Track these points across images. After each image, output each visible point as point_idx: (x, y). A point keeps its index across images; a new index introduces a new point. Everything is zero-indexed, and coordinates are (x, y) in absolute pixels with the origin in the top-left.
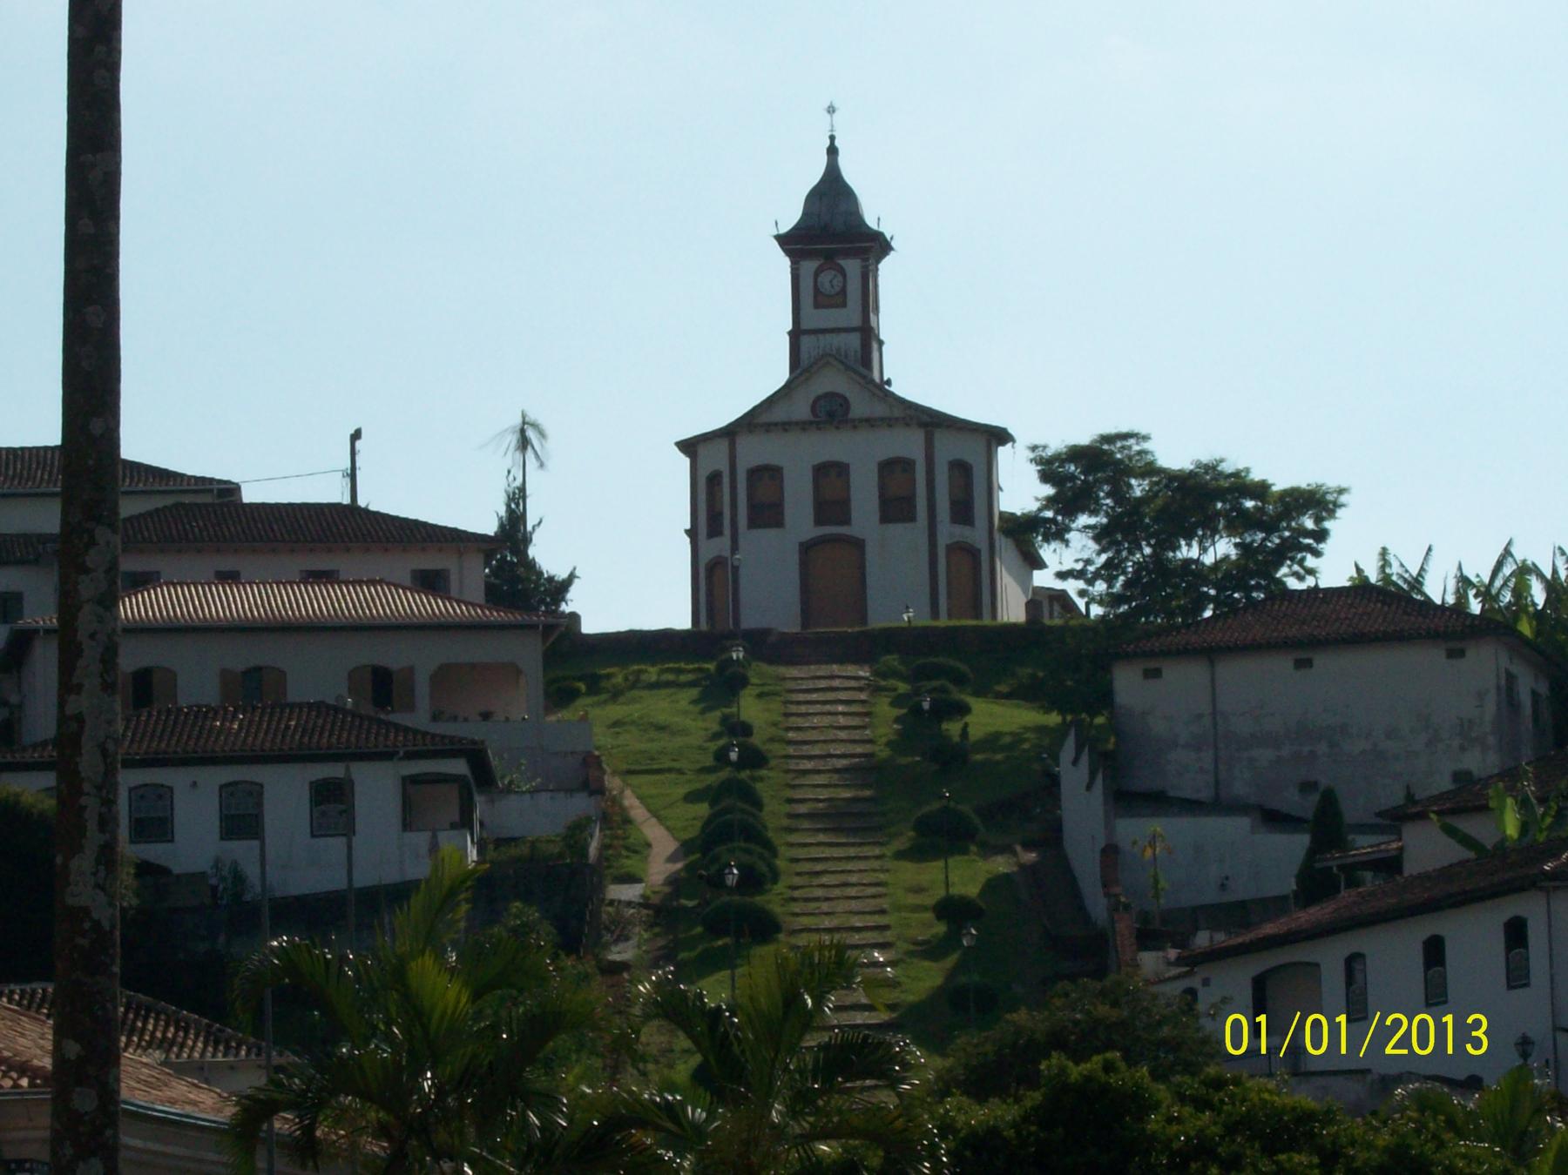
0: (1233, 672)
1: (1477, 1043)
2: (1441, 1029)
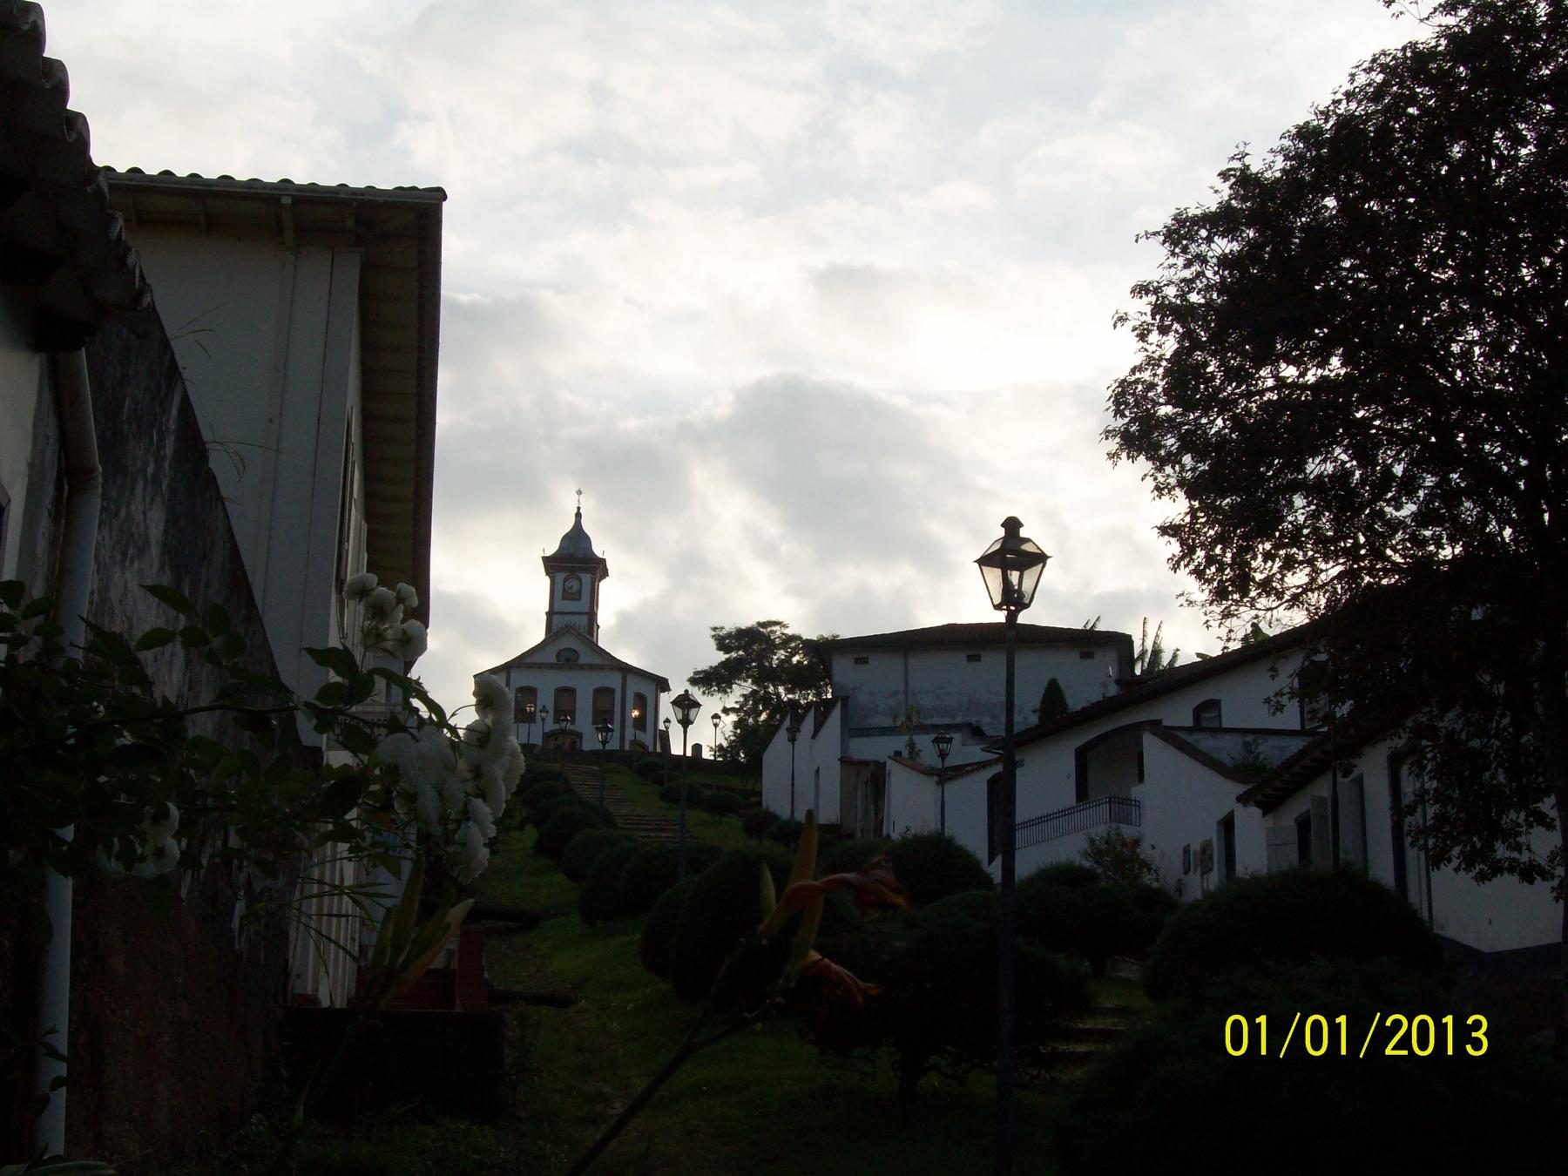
1: (1477, 1044)
2: (1441, 1030)
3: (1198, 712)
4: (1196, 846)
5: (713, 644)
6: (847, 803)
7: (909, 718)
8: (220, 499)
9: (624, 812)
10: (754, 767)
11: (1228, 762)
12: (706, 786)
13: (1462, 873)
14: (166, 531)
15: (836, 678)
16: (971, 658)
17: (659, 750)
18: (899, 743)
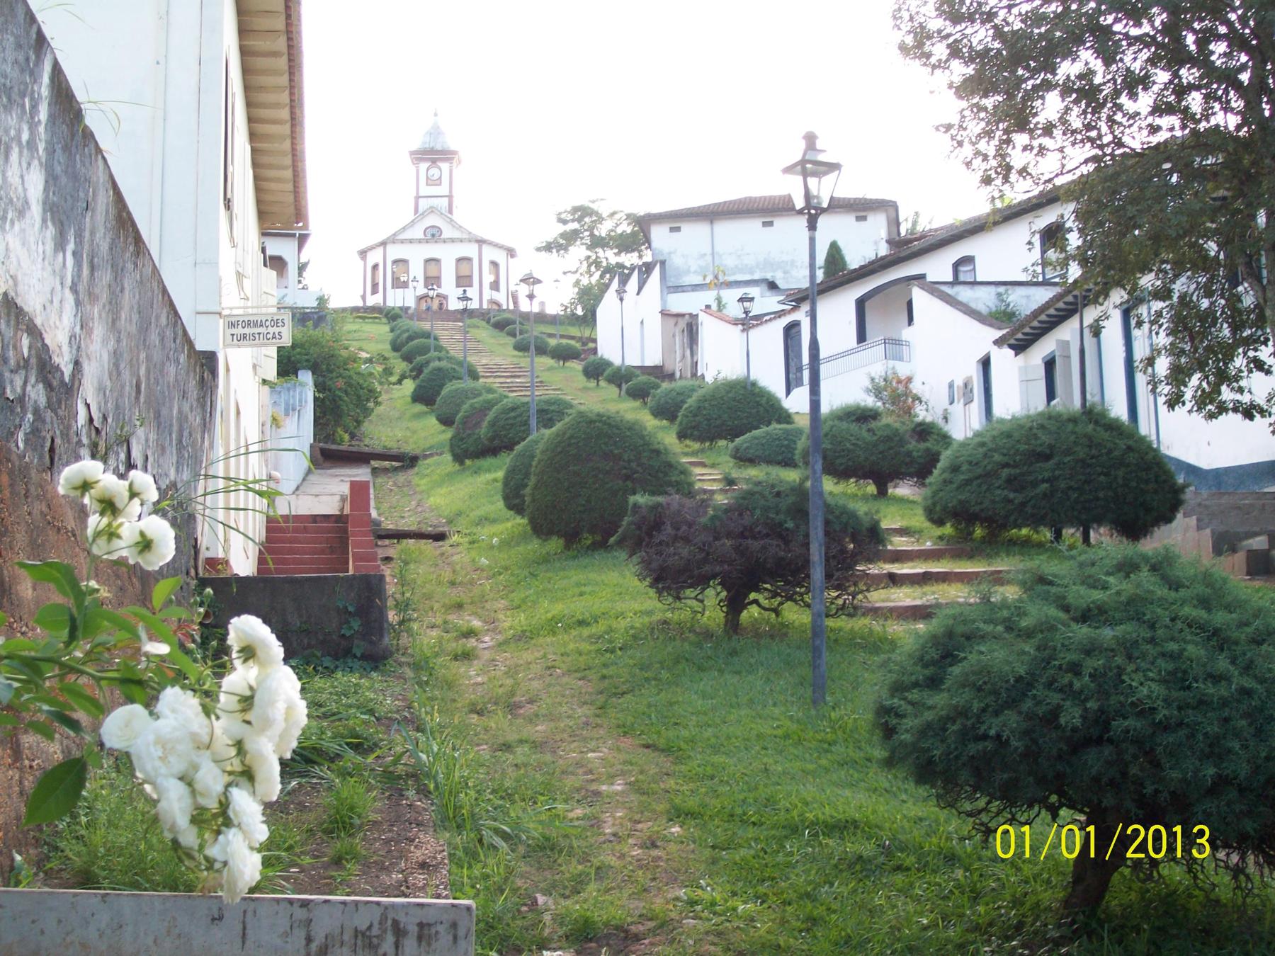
0: (579, 335)
3: (956, 266)
4: (959, 382)
6: (667, 349)
7: (716, 277)
8: (99, 150)
9: (484, 362)
10: (589, 319)
11: (984, 310)
12: (551, 335)
13: (1194, 414)
14: (46, 190)
15: (654, 245)
17: (511, 307)
18: (709, 297)
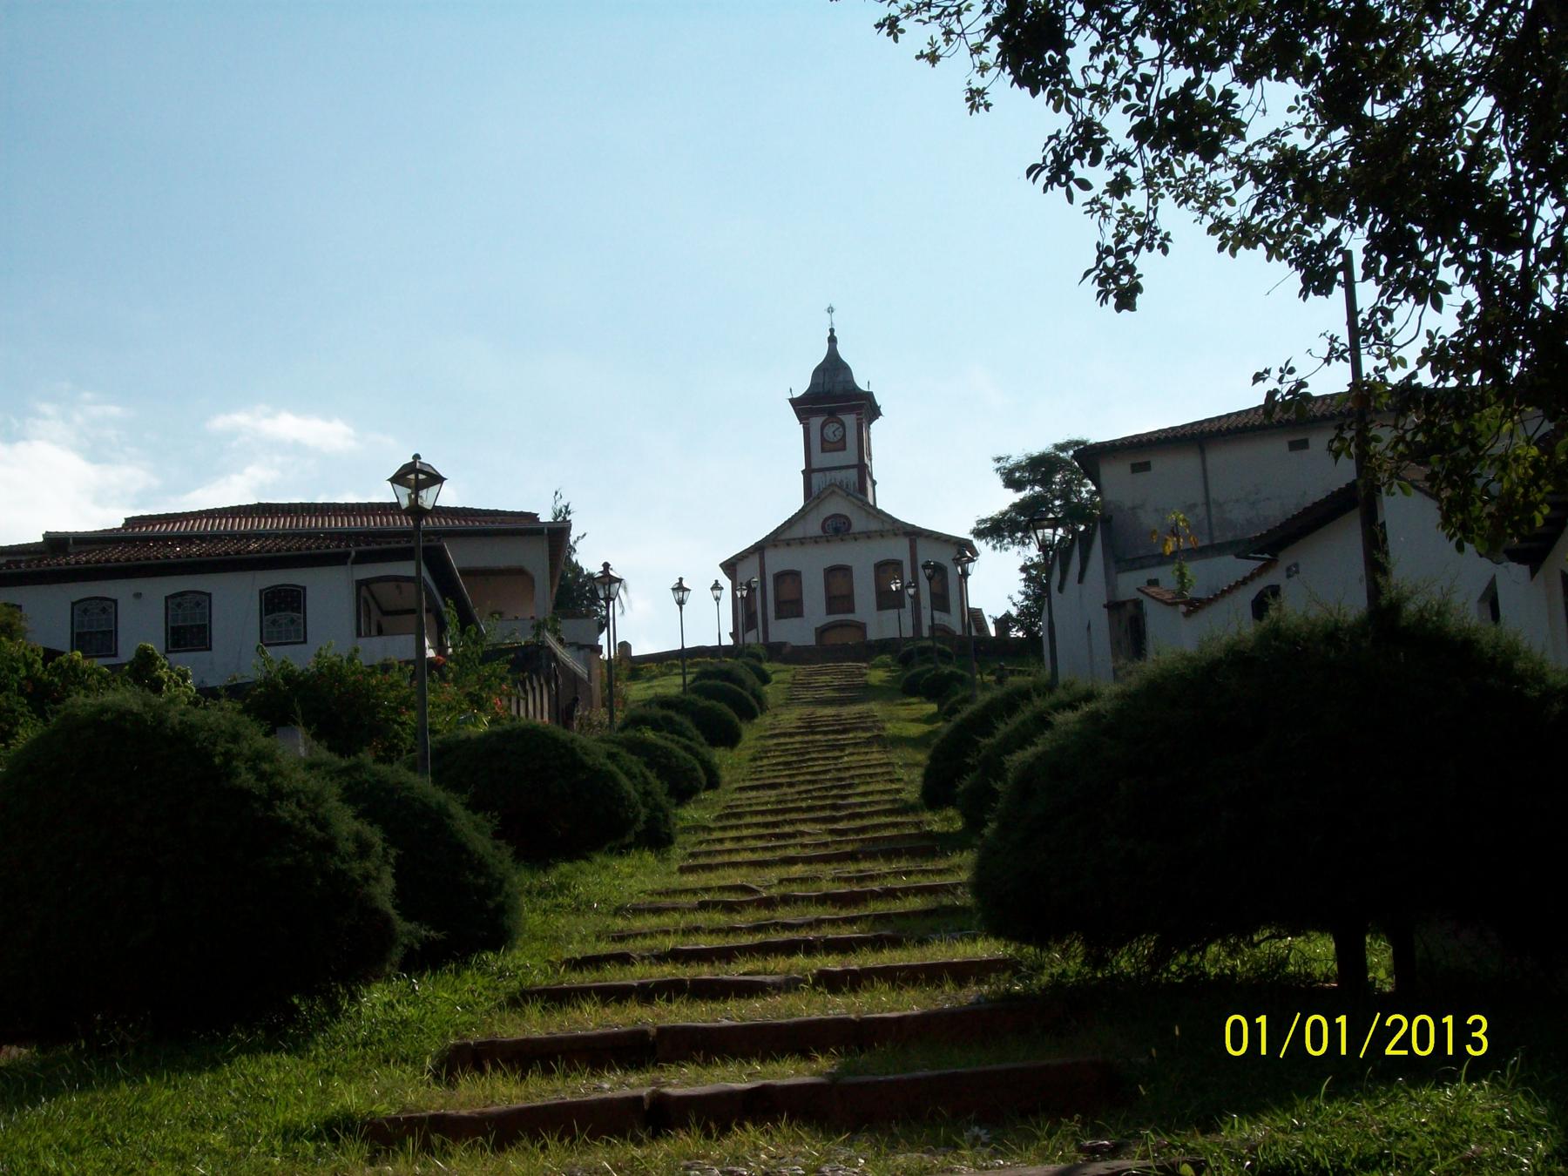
1: (1477, 1044)
2: (1441, 1030)
5: (998, 481)
16: (1296, 446)
